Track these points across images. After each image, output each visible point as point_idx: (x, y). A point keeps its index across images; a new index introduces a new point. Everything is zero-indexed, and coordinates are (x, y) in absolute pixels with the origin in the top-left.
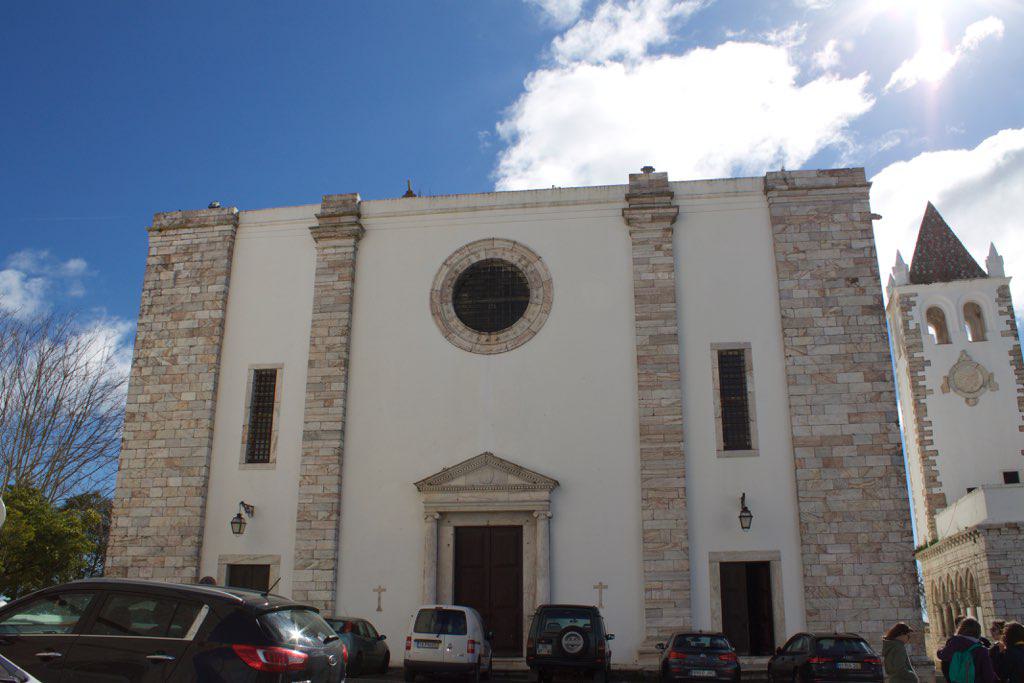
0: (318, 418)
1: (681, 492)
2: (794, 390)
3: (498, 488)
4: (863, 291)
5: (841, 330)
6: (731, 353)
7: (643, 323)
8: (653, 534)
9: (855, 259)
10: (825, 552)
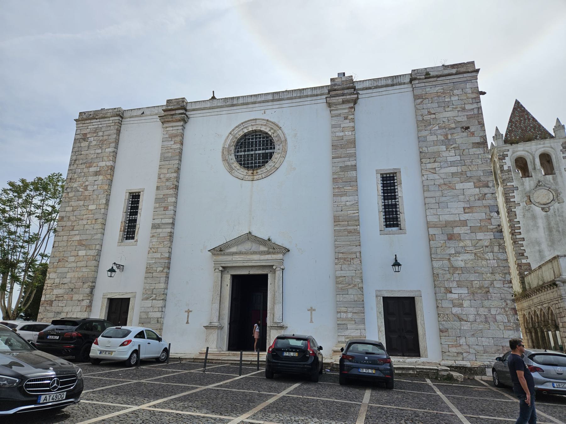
0: (161, 217)
1: (358, 254)
2: (427, 194)
3: (255, 253)
4: (473, 134)
5: (458, 158)
6: (388, 175)
7: (335, 160)
8: (341, 279)
9: (467, 115)
10: (451, 292)
